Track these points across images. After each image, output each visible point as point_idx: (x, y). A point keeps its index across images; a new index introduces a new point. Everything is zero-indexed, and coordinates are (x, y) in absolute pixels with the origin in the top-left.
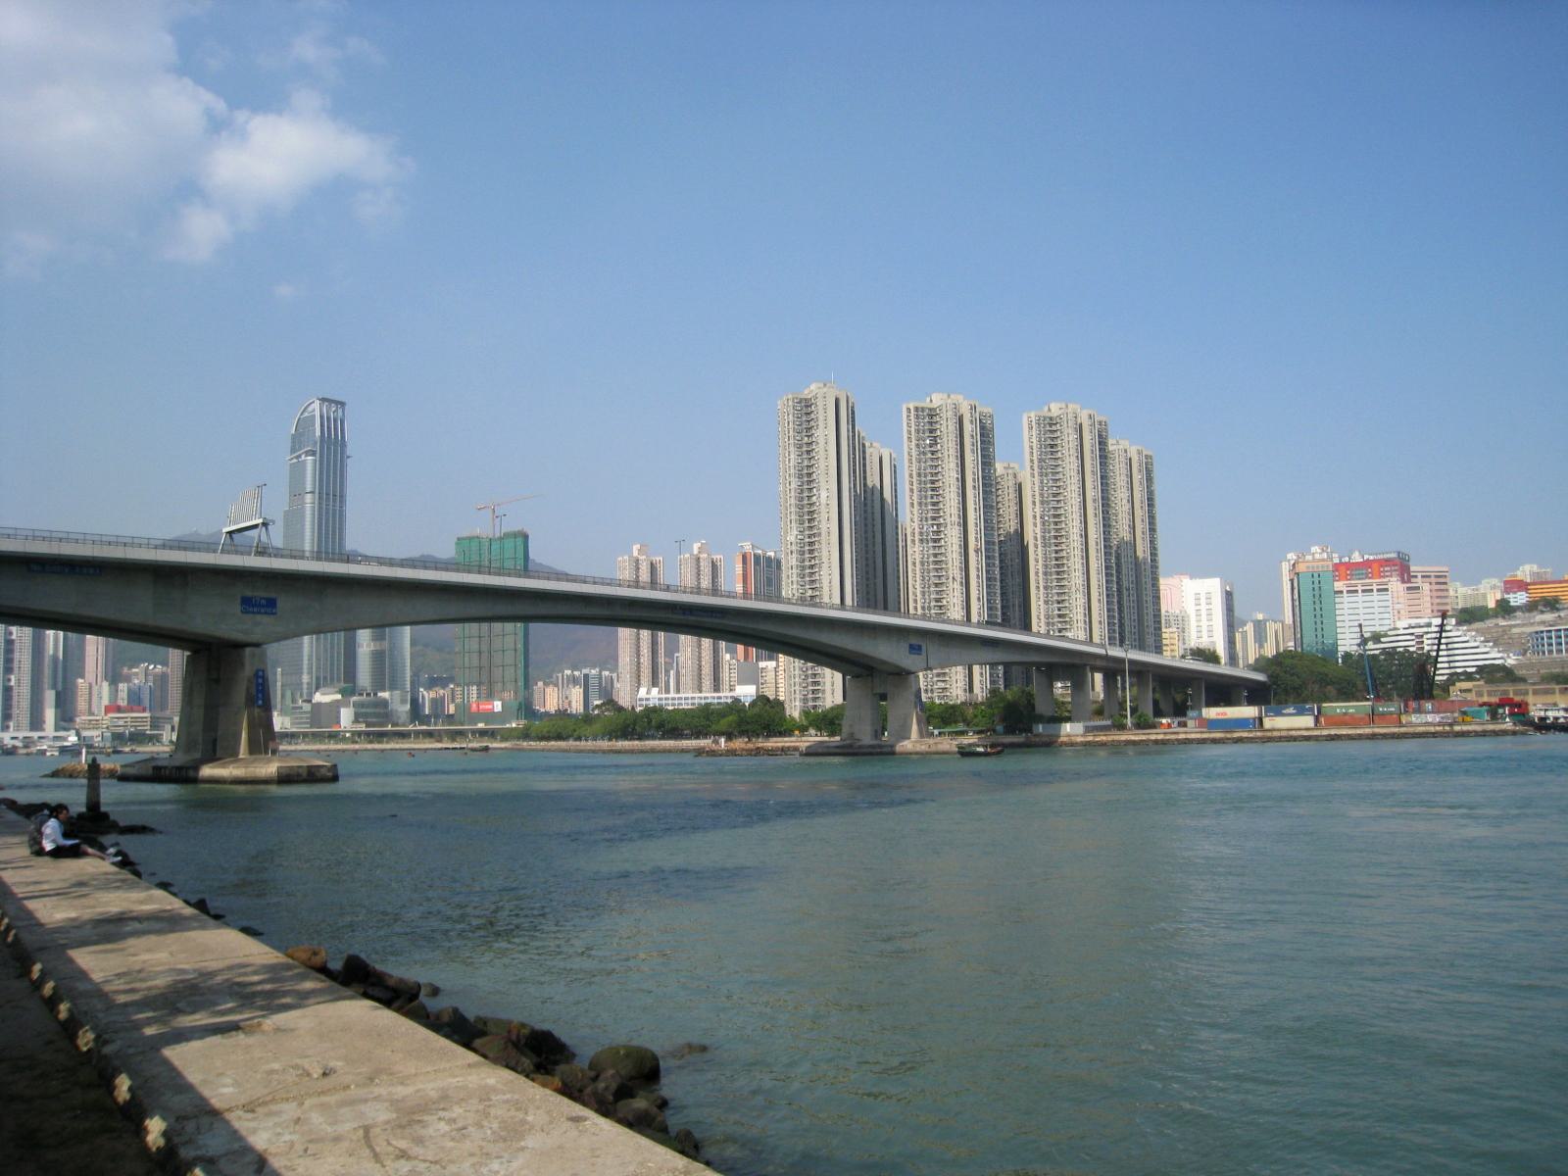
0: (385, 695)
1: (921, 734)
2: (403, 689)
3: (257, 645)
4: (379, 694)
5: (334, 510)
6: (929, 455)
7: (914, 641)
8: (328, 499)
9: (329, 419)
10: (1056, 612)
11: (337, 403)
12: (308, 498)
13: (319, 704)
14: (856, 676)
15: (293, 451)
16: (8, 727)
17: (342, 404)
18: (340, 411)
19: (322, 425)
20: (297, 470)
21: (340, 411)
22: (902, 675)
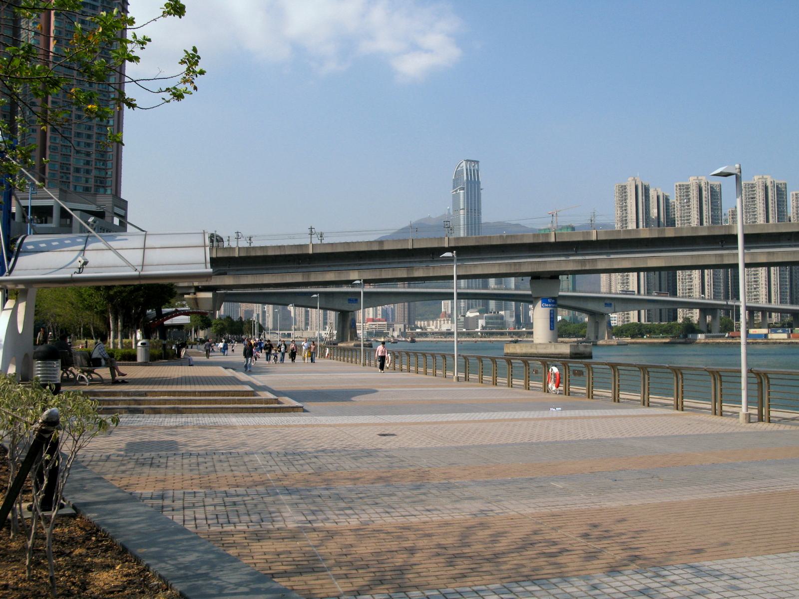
0: (502, 313)
1: (608, 338)
2: (511, 310)
3: (353, 312)
4: (500, 312)
5: (475, 217)
6: (686, 207)
7: (608, 302)
8: (471, 212)
9: (470, 170)
10: (753, 280)
11: (474, 161)
12: (462, 212)
13: (469, 317)
14: (591, 315)
15: (454, 188)
16: (326, 328)
17: (478, 162)
18: (476, 166)
19: (467, 174)
20: (456, 198)
21: (476, 166)
22: (602, 315)
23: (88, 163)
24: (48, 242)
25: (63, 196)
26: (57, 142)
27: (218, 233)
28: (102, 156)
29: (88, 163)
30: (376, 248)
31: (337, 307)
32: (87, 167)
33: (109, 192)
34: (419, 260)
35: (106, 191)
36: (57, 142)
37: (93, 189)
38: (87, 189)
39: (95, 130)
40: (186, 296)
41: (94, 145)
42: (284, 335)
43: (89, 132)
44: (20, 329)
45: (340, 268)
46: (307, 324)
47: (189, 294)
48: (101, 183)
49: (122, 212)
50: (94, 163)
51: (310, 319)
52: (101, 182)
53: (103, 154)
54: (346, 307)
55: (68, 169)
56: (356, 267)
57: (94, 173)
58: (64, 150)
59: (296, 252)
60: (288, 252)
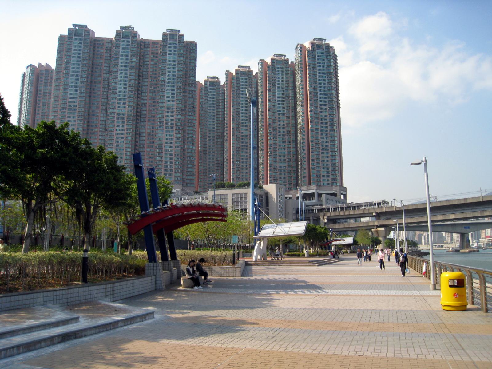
3: (467, 233)
23: (328, 172)
24: (268, 227)
25: (319, 186)
26: (314, 165)
27: (385, 200)
28: (334, 169)
29: (328, 172)
30: (463, 202)
31: (458, 231)
32: (328, 174)
33: (338, 184)
34: (487, 207)
35: (336, 184)
36: (314, 165)
37: (331, 184)
38: (328, 184)
39: (330, 158)
40: (372, 230)
41: (330, 165)
42: (439, 247)
43: (327, 159)
44: (261, 247)
45: (446, 213)
46: (452, 240)
47: (374, 229)
48: (334, 181)
49: (344, 193)
50: (330, 172)
51: (453, 237)
52: (334, 180)
53: (334, 168)
54: (463, 231)
55: (320, 176)
56: (454, 212)
57: (331, 177)
58: (318, 168)
59: (414, 208)
60: (419, 207)
